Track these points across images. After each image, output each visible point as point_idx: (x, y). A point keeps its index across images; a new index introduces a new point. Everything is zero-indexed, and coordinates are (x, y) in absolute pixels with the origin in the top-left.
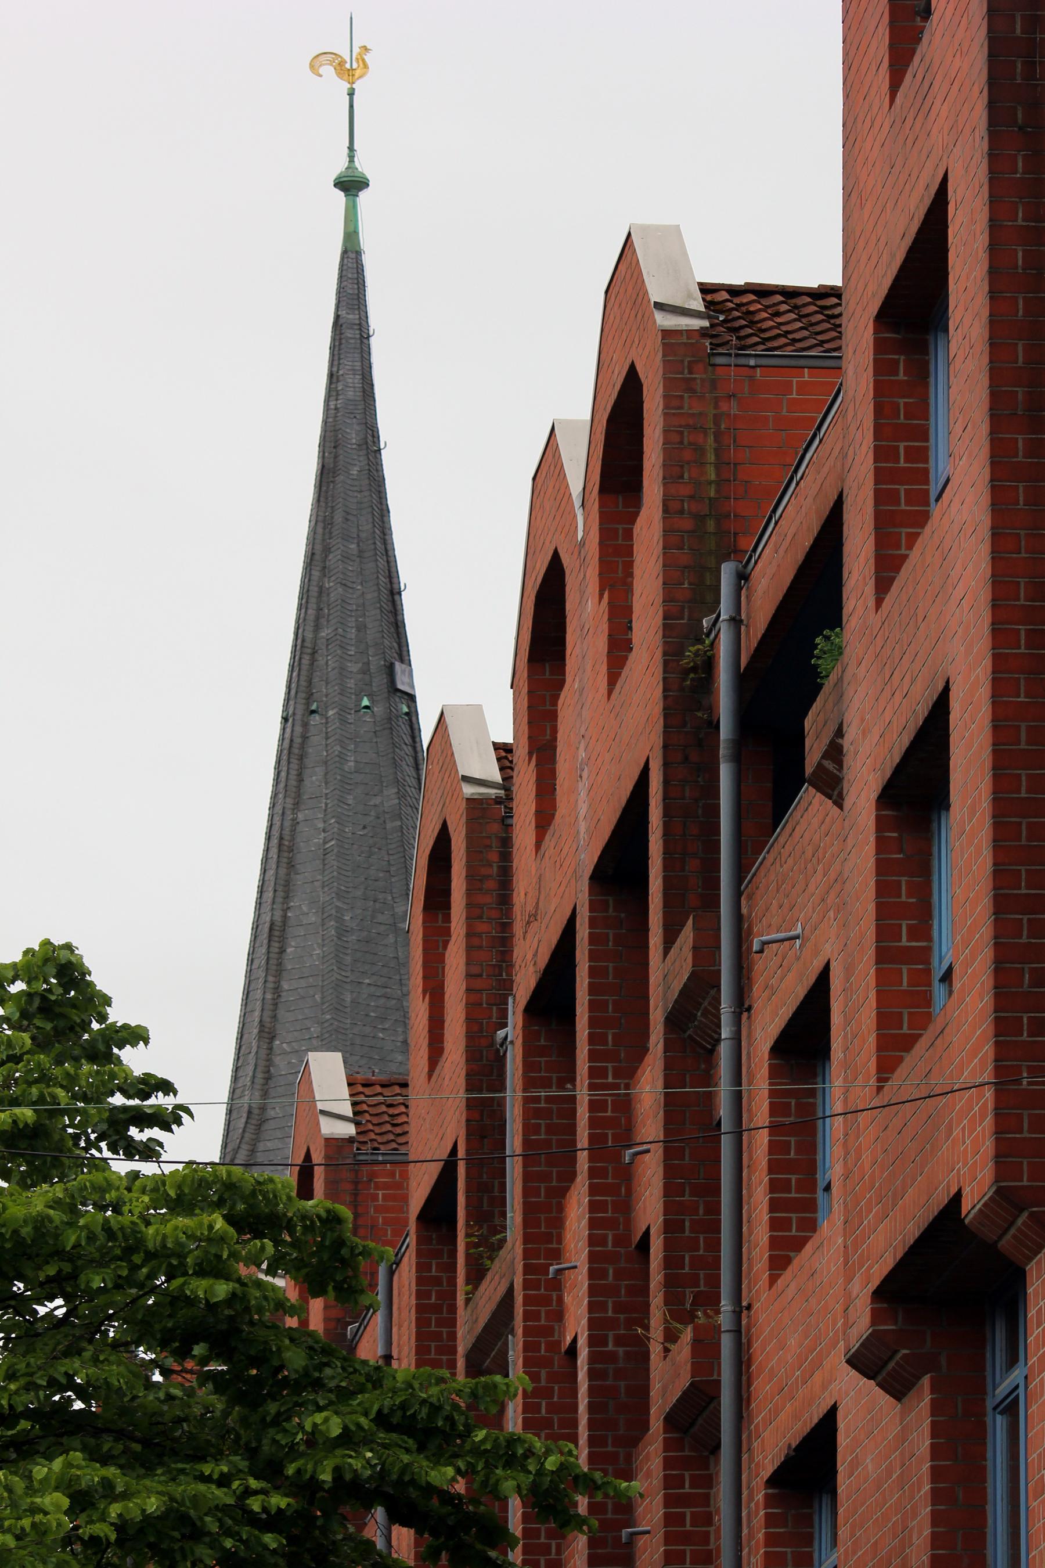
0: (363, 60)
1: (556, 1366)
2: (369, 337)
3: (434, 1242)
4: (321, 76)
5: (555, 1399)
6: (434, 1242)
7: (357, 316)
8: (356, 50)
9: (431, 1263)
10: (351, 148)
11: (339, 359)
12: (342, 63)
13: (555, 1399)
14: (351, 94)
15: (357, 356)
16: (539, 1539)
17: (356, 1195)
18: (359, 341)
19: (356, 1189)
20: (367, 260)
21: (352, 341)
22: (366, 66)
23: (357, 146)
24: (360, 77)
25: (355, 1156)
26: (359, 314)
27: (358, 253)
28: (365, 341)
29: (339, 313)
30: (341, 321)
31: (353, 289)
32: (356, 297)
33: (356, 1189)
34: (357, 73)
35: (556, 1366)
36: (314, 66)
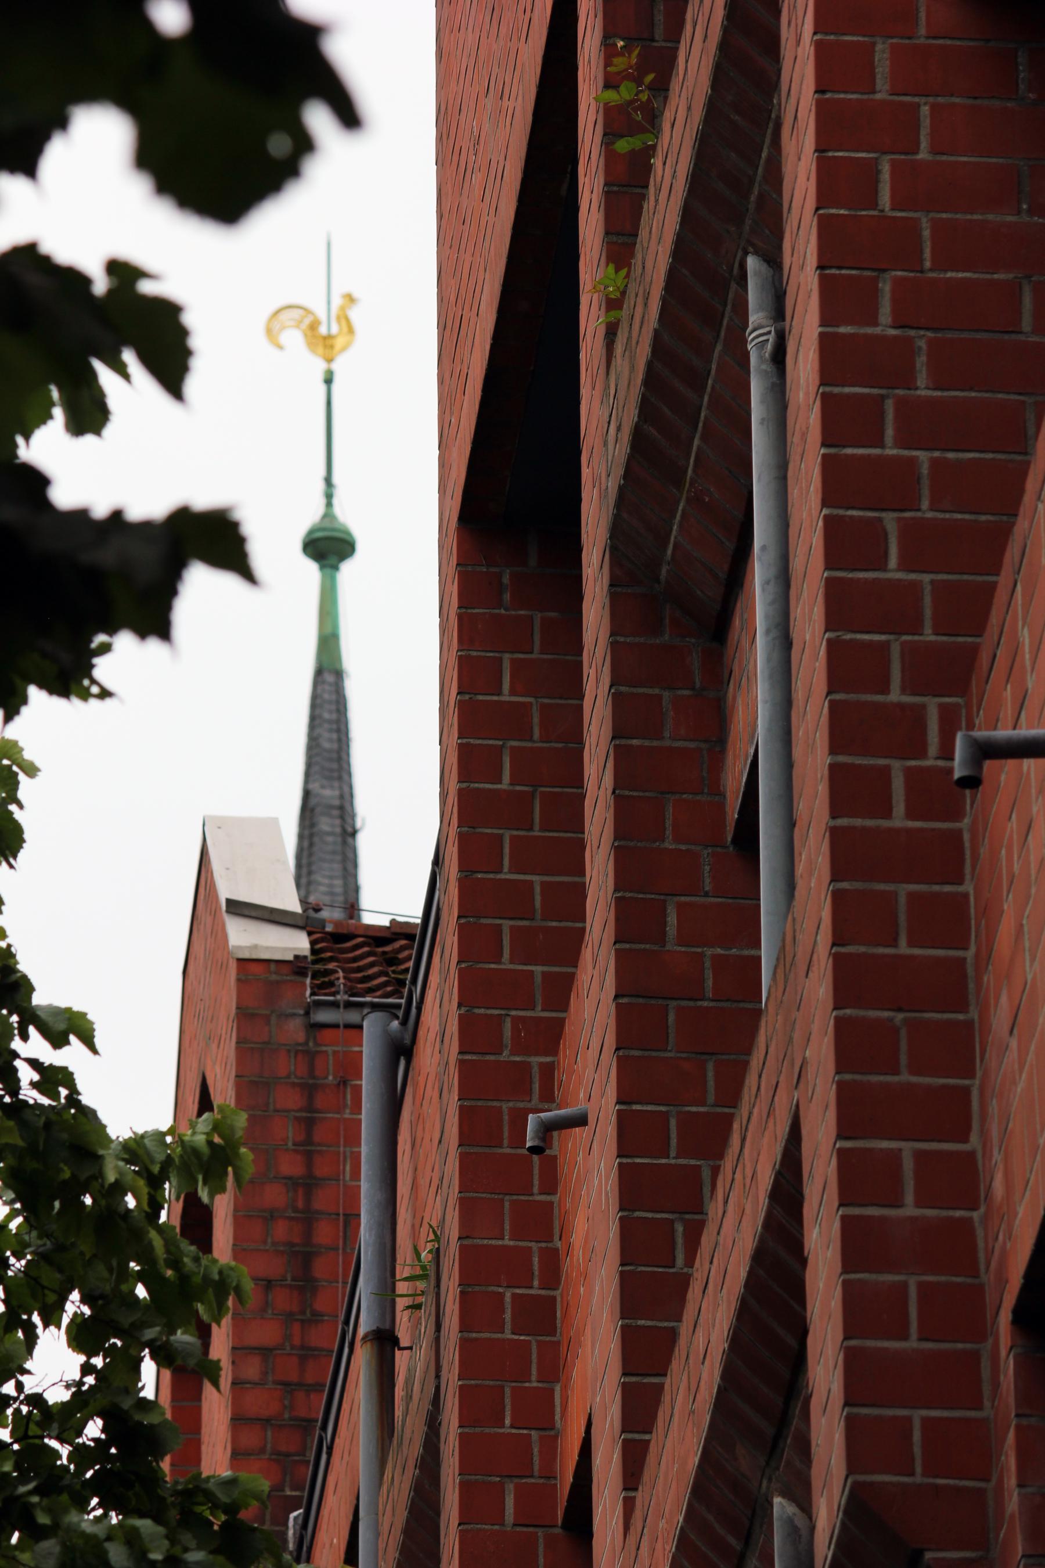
0: (348, 320)
1: (922, 31)
2: (354, 833)
3: (507, 597)
4: (280, 347)
5: (923, 155)
6: (507, 597)
7: (337, 793)
8: (337, 302)
9: (501, 660)
10: (328, 481)
11: (310, 873)
12: (314, 326)
13: (923, 155)
14: (329, 381)
15: (337, 866)
16: (885, 690)
17: (309, 1124)
18: (339, 839)
19: (310, 1108)
20: (354, 689)
21: (330, 839)
22: (351, 330)
23: (336, 479)
24: (344, 349)
25: (307, 1013)
26: (341, 788)
27: (339, 675)
28: (350, 840)
29: (311, 786)
30: (313, 801)
31: (330, 740)
32: (335, 756)
33: (310, 1108)
34: (339, 342)
35: (922, 31)
36: (271, 333)
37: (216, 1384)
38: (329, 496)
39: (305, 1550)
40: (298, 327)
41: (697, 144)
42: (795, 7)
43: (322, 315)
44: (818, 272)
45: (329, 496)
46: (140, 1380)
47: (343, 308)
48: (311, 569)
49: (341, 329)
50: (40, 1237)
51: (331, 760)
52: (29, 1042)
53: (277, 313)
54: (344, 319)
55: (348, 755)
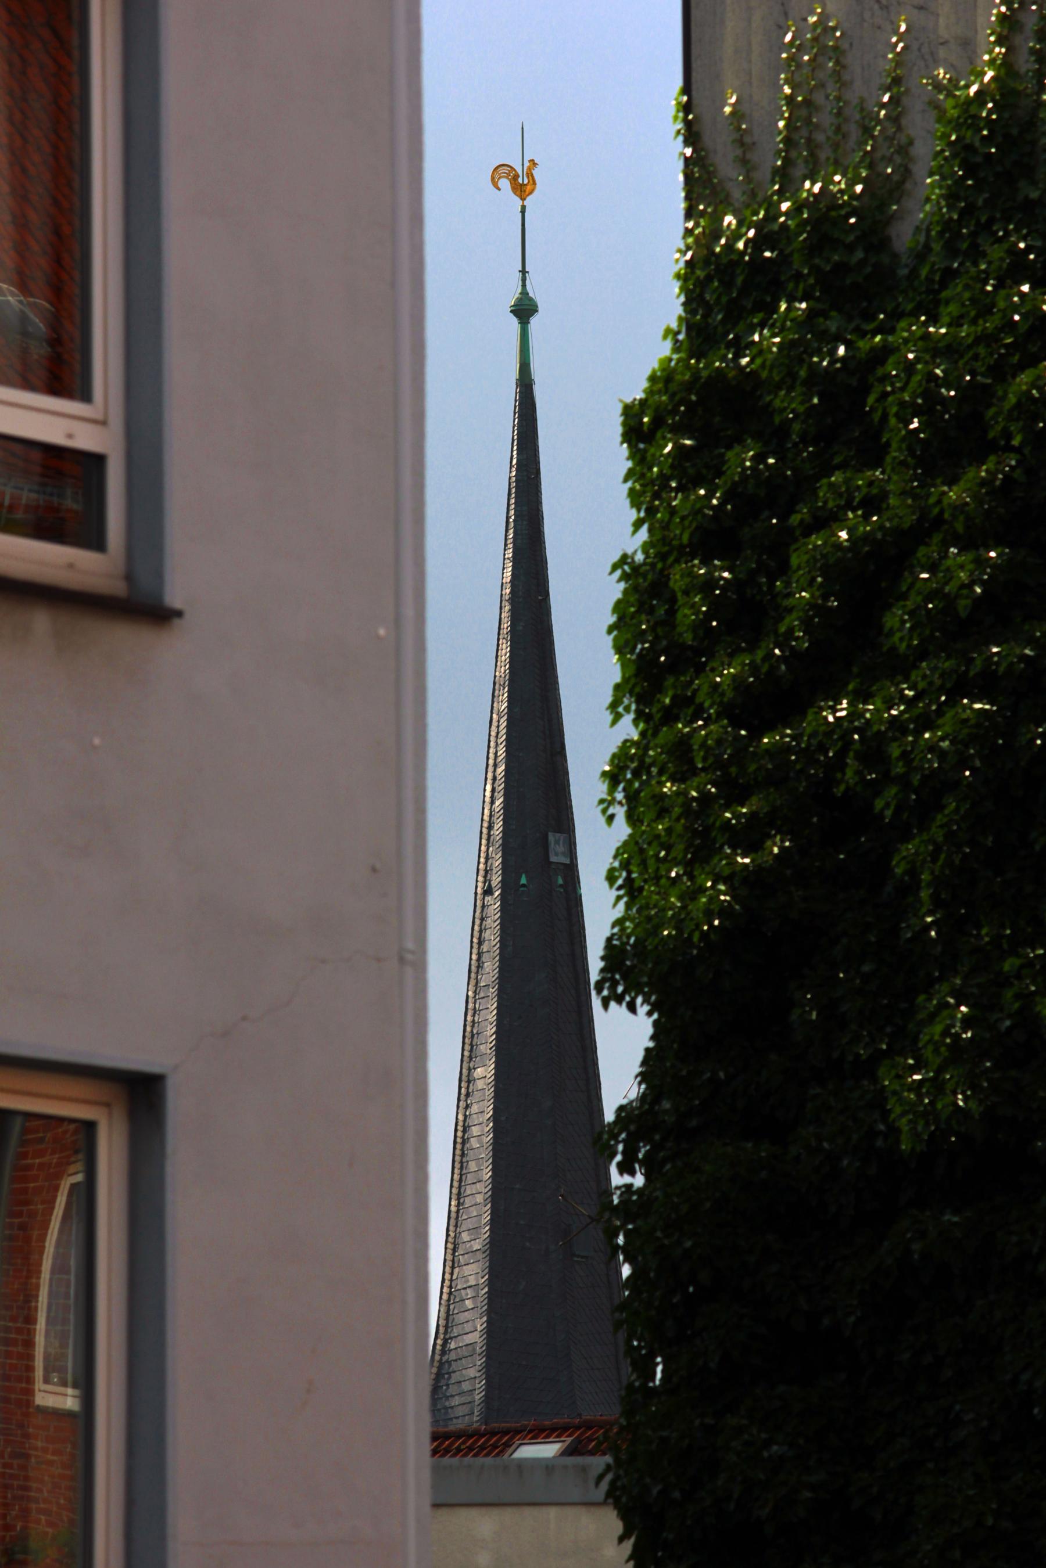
4: (499, 189)
8: (527, 164)
22: (534, 183)
24: (530, 193)
38: (524, 280)
40: (507, 177)
43: (520, 173)
44: (629, 484)
45: (524, 280)
46: (615, 640)
47: (529, 169)
48: (514, 321)
49: (529, 182)
50: (1036, 61)
51: (638, 816)
54: (530, 175)
55: (538, 442)
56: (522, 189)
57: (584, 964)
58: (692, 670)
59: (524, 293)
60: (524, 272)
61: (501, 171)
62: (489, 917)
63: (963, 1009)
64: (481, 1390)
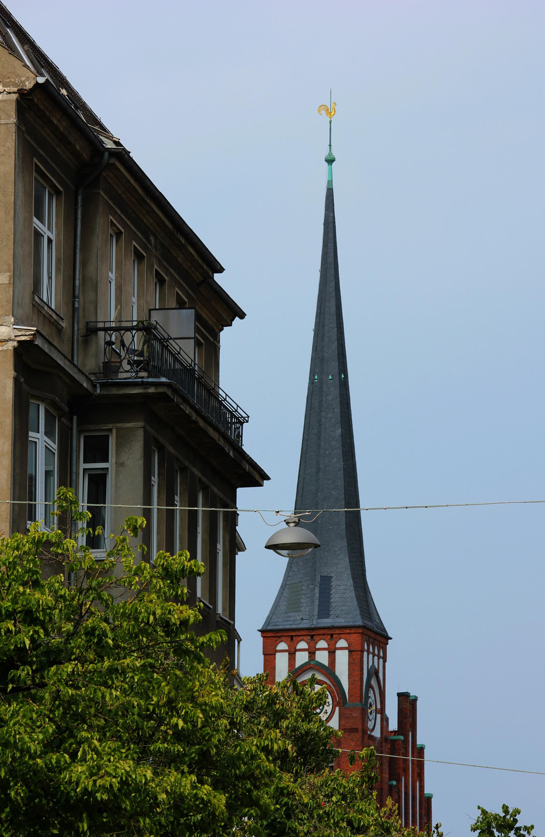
4: (321, 115)
12: (327, 110)
36: (319, 111)
37: (177, 496)
38: (330, 149)
39: (332, 836)
41: (155, 480)
42: (77, 457)
45: (330, 149)
48: (335, 154)
52: (396, 694)
53: (320, 106)
56: (329, 113)
57: (13, 490)
58: (90, 790)
59: (330, 154)
60: (330, 145)
61: (323, 107)
62: (374, 642)
63: (55, 832)
64: (27, 333)
